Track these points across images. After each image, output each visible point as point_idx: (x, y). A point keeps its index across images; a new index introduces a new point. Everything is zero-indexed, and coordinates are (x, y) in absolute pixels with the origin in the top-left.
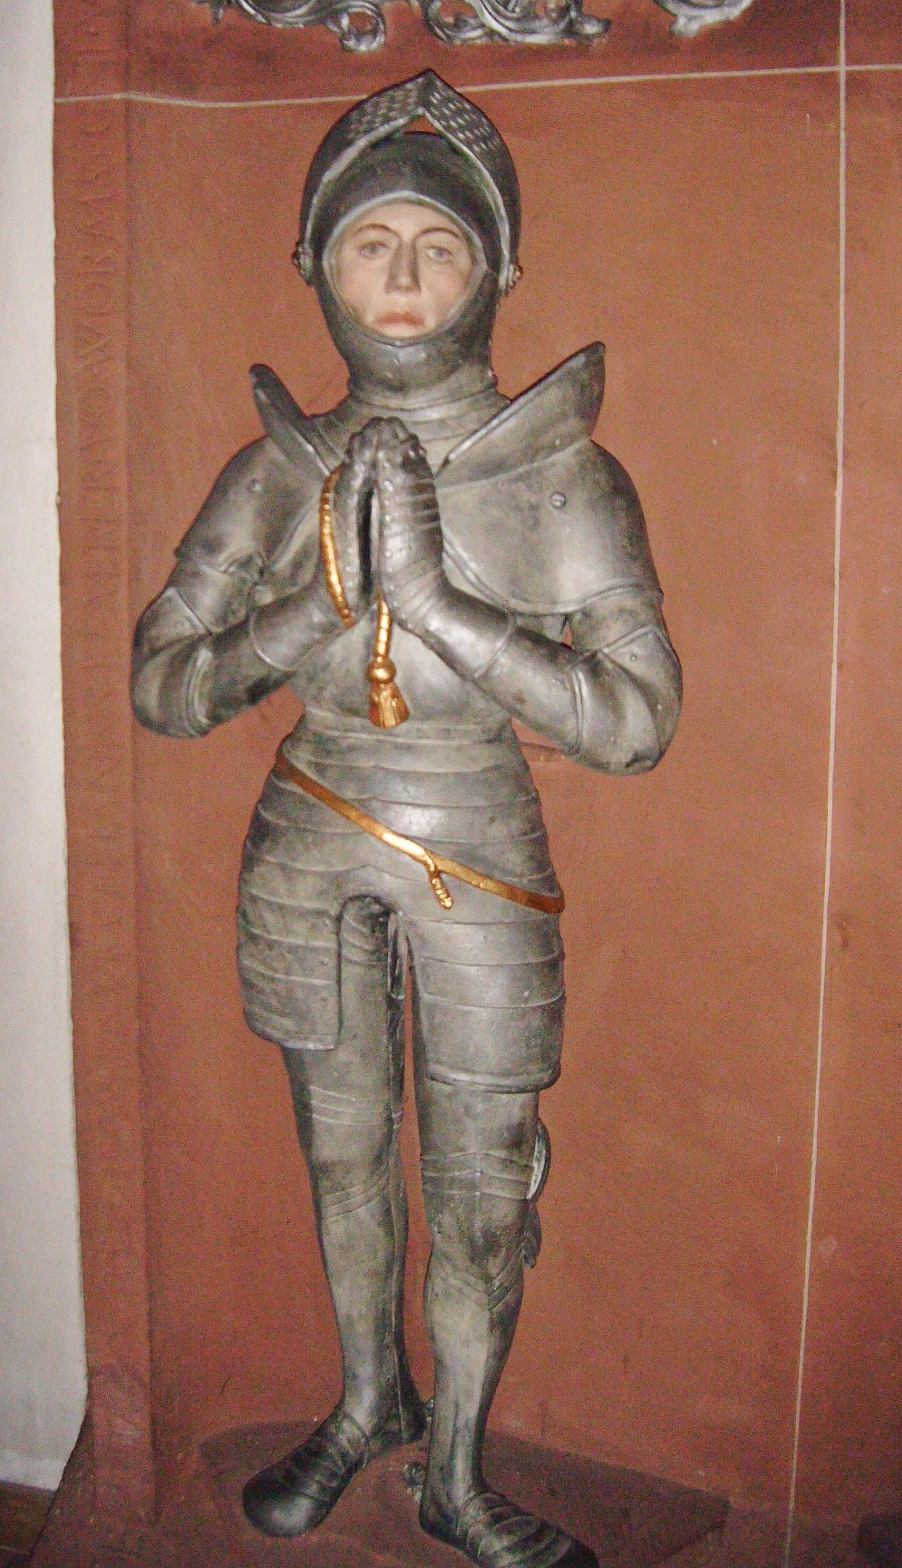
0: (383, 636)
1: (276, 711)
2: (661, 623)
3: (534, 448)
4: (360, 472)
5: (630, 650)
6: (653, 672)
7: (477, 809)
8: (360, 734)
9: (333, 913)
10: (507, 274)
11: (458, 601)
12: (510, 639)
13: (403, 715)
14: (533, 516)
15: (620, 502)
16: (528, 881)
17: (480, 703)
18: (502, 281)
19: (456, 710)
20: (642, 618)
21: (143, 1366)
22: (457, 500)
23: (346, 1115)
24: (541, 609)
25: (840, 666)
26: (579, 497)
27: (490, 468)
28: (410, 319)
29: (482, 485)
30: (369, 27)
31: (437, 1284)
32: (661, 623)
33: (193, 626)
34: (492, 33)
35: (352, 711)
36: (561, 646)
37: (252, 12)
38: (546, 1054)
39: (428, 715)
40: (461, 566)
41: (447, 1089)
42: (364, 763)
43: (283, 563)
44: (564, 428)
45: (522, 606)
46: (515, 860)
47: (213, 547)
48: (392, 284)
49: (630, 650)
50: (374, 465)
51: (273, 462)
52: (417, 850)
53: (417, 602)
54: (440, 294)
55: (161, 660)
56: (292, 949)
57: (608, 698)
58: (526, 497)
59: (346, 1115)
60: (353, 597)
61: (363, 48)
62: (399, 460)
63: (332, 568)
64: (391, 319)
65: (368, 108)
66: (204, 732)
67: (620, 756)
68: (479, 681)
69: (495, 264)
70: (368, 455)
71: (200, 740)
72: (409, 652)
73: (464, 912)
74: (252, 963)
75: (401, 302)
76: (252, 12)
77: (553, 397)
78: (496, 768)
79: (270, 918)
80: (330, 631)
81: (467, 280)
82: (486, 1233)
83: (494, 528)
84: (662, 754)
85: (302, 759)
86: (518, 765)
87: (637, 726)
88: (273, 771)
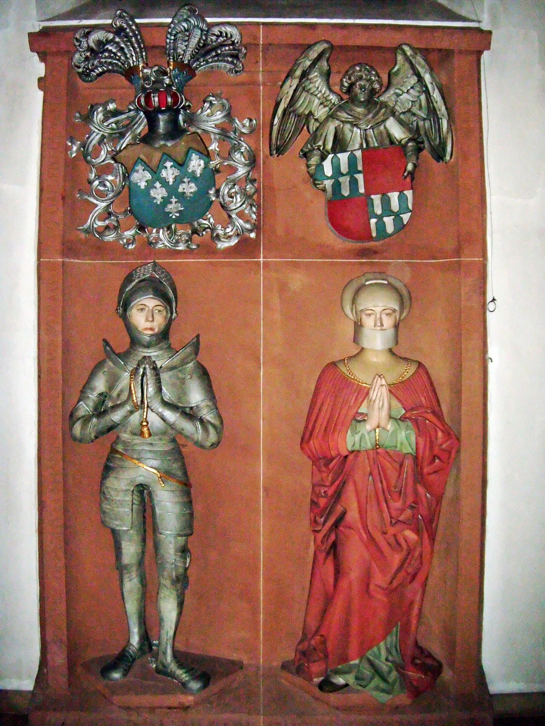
0: (145, 413)
1: (112, 435)
2: (217, 408)
3: (184, 362)
4: (141, 371)
5: (209, 416)
6: (217, 422)
7: (169, 460)
8: (137, 440)
9: (132, 489)
10: (174, 315)
11: (166, 404)
12: (181, 414)
13: (150, 435)
14: (183, 381)
15: (205, 377)
16: (183, 479)
17: (170, 431)
18: (173, 317)
19: (164, 433)
20: (212, 407)
21: (65, 638)
22: (165, 377)
23: (130, 550)
24: (186, 405)
25: (263, 420)
26: (195, 376)
27: (172, 368)
28: (151, 329)
29: (170, 373)
30: (131, 242)
31: (162, 595)
32: (217, 408)
33: (88, 412)
34: (166, 246)
35: (135, 434)
36: (190, 414)
37: (98, 236)
38: (189, 527)
39: (156, 435)
40: (166, 395)
41: (164, 536)
42: (137, 448)
43: (115, 394)
44: (191, 357)
45: (181, 405)
46: (179, 473)
47: (93, 389)
48: (147, 320)
49: (209, 416)
50: (145, 369)
51: (110, 366)
52: (155, 471)
53: (156, 405)
54: (159, 323)
55: (79, 422)
56: (119, 501)
57: (205, 429)
58: (180, 375)
59: (130, 550)
60: (139, 403)
61: (130, 248)
62: (152, 367)
63: (134, 396)
64: (146, 329)
65: (138, 270)
66: (92, 441)
67: (209, 444)
68: (172, 426)
69: (172, 314)
70: (143, 366)
71: (91, 444)
72: (153, 418)
73: (167, 488)
74: (121, 503)
75: (149, 325)
76: (98, 236)
77: (188, 350)
78: (173, 449)
79: (113, 493)
80: (131, 412)
81: (165, 318)
82: (177, 577)
83: (174, 385)
84: (219, 443)
85: (120, 448)
86: (177, 449)
87: (213, 437)
88: (110, 452)
